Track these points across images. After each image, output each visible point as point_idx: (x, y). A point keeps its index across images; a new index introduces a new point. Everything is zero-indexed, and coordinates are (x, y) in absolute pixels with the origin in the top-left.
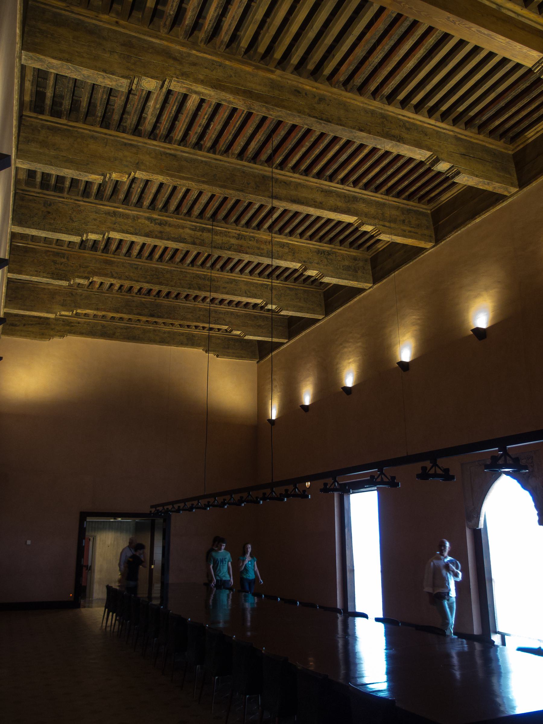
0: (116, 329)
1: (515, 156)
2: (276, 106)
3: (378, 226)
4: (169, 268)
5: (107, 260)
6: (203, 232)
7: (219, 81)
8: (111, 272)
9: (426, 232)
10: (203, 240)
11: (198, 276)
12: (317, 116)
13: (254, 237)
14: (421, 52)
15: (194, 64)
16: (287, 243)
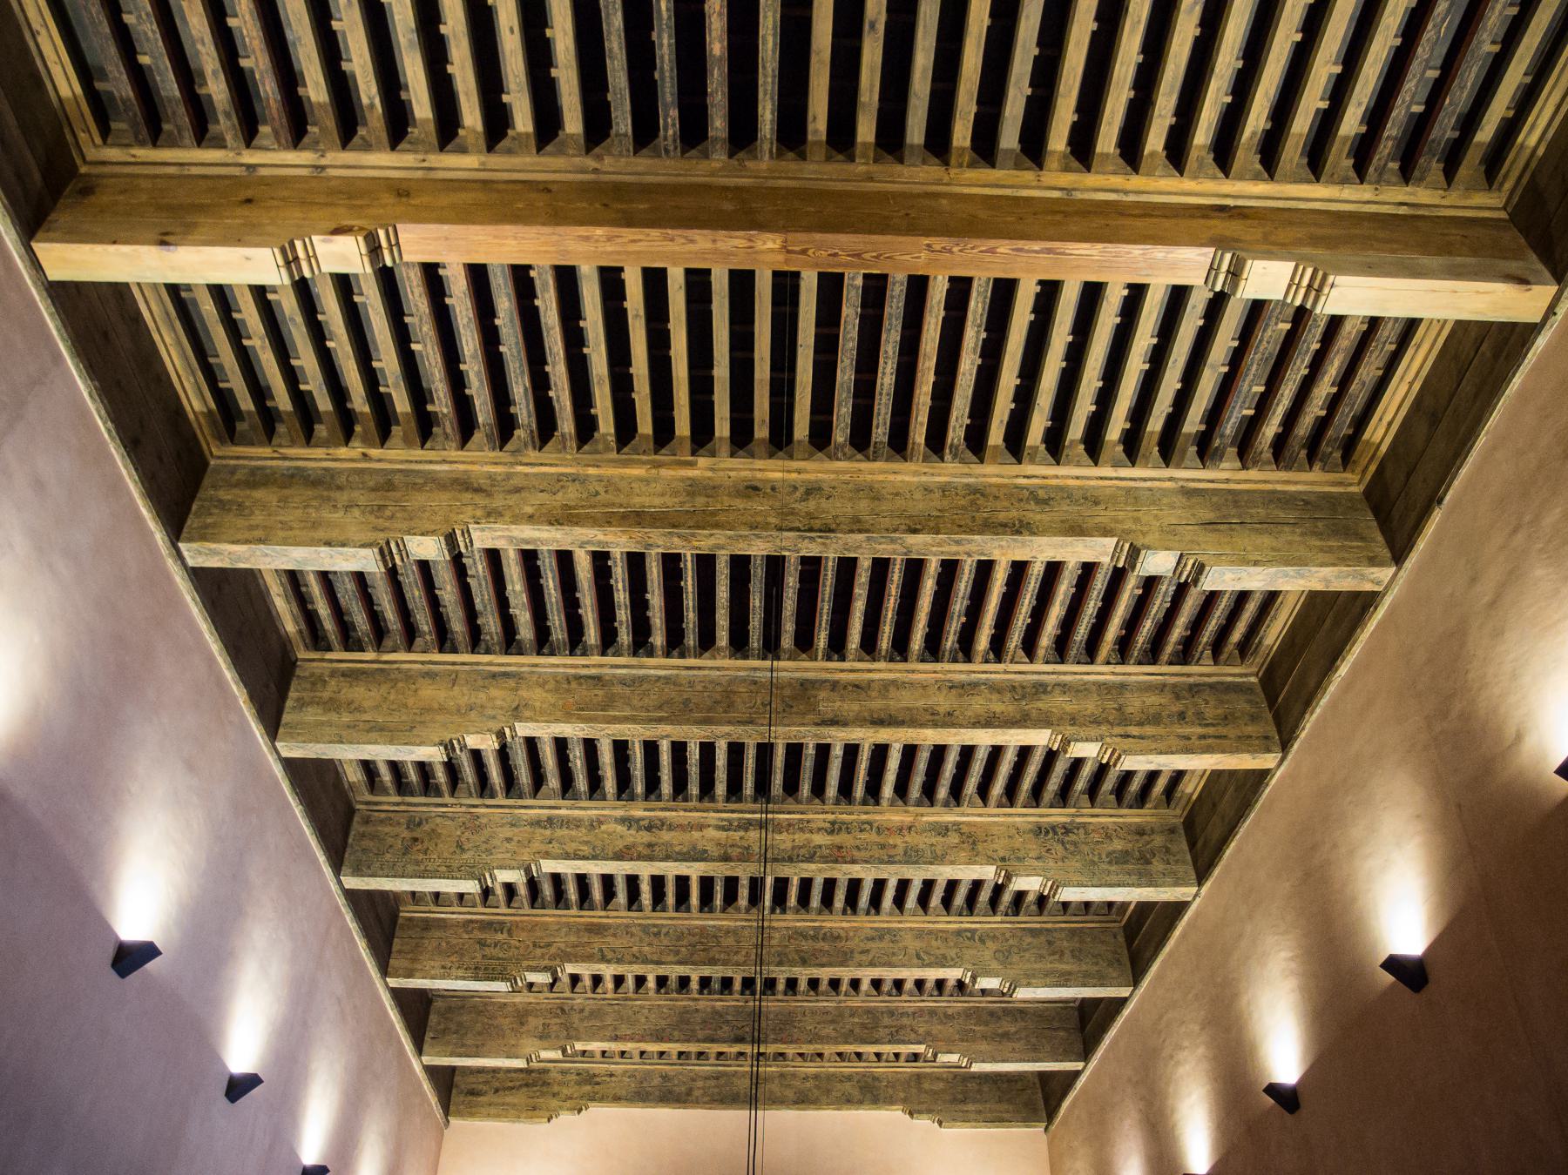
0: (693, 1080)
1: (1368, 494)
2: (699, 527)
3: (1108, 740)
4: (732, 924)
5: (592, 924)
6: (746, 830)
7: (570, 508)
8: (601, 950)
9: (1250, 729)
10: (747, 848)
11: (802, 934)
12: (797, 524)
13: (870, 823)
14: (973, 336)
15: (518, 490)
16: (955, 824)
